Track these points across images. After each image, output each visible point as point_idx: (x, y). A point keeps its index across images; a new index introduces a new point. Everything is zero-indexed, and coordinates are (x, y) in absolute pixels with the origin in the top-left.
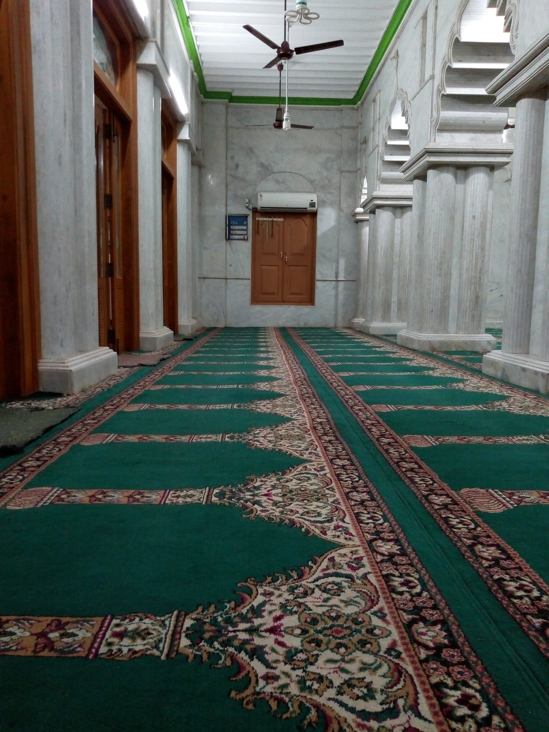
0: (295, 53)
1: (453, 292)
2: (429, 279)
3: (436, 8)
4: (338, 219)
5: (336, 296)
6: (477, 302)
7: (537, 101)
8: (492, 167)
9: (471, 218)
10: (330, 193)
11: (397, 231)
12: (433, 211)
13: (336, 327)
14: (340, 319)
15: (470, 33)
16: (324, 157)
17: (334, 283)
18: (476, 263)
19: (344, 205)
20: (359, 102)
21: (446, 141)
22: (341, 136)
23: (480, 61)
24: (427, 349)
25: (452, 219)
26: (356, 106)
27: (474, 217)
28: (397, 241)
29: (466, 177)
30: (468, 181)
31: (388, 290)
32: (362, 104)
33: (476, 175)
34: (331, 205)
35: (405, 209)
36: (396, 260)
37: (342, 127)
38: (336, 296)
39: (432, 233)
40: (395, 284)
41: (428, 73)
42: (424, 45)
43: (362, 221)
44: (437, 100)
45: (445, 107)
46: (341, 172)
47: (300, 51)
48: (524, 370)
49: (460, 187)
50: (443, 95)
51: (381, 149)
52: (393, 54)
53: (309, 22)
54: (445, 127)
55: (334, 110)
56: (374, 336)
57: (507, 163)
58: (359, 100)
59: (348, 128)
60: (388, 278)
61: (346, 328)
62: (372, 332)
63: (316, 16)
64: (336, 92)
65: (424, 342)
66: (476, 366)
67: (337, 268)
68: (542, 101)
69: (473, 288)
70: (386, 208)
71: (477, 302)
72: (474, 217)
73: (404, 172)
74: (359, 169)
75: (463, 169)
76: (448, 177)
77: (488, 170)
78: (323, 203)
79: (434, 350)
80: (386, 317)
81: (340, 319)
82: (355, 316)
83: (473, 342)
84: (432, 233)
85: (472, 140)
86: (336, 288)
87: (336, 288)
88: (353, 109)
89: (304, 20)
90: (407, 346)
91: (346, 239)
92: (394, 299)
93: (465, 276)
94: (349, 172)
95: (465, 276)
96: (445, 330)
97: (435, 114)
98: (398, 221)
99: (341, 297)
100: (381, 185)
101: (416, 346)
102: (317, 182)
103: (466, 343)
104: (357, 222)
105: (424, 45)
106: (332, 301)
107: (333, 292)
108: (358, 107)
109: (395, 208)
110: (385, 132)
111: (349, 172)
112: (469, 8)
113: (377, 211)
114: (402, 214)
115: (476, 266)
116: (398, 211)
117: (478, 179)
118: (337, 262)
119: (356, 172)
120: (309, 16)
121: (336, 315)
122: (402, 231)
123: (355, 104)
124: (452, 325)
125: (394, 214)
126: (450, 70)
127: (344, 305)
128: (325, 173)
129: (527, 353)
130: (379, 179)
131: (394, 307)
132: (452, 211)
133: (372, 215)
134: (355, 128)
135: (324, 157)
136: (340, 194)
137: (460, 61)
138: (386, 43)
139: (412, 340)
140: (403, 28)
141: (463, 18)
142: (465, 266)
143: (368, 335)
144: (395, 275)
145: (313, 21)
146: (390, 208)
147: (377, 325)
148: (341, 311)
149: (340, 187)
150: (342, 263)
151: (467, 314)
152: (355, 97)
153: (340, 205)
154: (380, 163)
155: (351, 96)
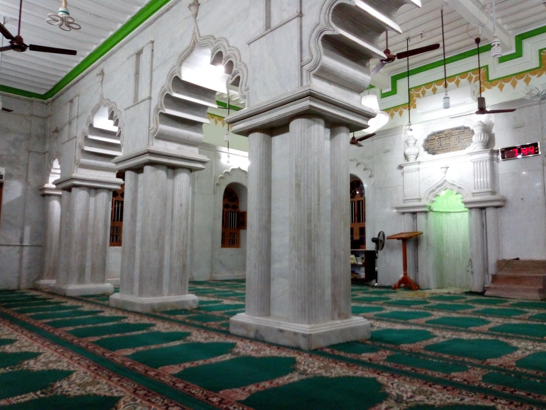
0: (28, 48)
1: (166, 262)
2: (149, 252)
3: (153, 51)
4: (25, 192)
5: (21, 259)
6: (184, 269)
7: (267, 136)
8: (191, 170)
9: (179, 205)
10: (18, 169)
11: (92, 207)
12: (151, 198)
13: (19, 289)
14: (24, 281)
15: (188, 75)
16: (12, 137)
17: (18, 248)
18: (183, 239)
19: (31, 180)
20: (50, 99)
21: (160, 146)
22: (31, 122)
23: (190, 96)
24: (149, 310)
25: (165, 205)
26: (46, 101)
27: (181, 205)
28: (91, 215)
29: (174, 175)
30: (176, 178)
31: (83, 256)
32: (53, 101)
33: (180, 175)
34: (19, 178)
35: (99, 190)
36: (90, 230)
37: (32, 115)
38: (21, 259)
39: (151, 215)
40: (89, 251)
41: (143, 94)
42: (137, 73)
43: (49, 195)
44: (155, 117)
45: (162, 122)
46: (29, 152)
47: (33, 48)
48: (281, 331)
49: (170, 181)
50: (161, 114)
51: (80, 140)
52: (97, 71)
53: (69, 29)
54: (162, 137)
55: (25, 100)
56: (71, 298)
57: (203, 169)
58: (50, 97)
59: (37, 117)
60: (84, 247)
61: (31, 289)
62: (68, 294)
63: (78, 27)
64: (31, 86)
65: (147, 305)
66: (106, 303)
67: (22, 234)
68: (269, 137)
69: (181, 259)
70: (83, 188)
71: (184, 269)
72: (181, 205)
73: (116, 163)
74: (47, 152)
75: (173, 169)
76: (162, 173)
77: (189, 171)
78: (10, 176)
79: (154, 311)
80: (81, 280)
81: (24, 281)
82: (40, 277)
83: (183, 302)
84: (151, 215)
85: (179, 148)
86: (21, 252)
87: (21, 252)
88: (43, 103)
89: (64, 27)
90: (125, 308)
91: (32, 210)
92: (88, 264)
93: (175, 250)
94: (37, 153)
95: (175, 250)
96: (161, 294)
97: (152, 125)
98: (92, 200)
99: (25, 261)
100: (79, 169)
101: (138, 309)
102: (4, 157)
103: (178, 303)
104: (44, 195)
105: (137, 73)
106: (16, 264)
107: (17, 256)
108: (49, 103)
109: (90, 188)
110: (87, 128)
111: (37, 153)
112: (188, 59)
113: (74, 189)
114: (96, 194)
115: (183, 242)
116: (93, 191)
117: (183, 178)
118: (23, 229)
119: (44, 153)
120: (71, 25)
121: (19, 277)
122: (96, 207)
123: (46, 99)
124: (166, 290)
125: (89, 192)
126: (168, 96)
127: (29, 268)
128: (13, 151)
129: (268, 315)
130: (77, 164)
131: (88, 270)
132: (166, 199)
133: (66, 193)
134: (45, 118)
135: (12, 137)
136: (27, 170)
137: (177, 92)
138: (90, 62)
139: (133, 304)
140: (110, 55)
141: (183, 64)
142: (175, 242)
143: (65, 296)
144: (89, 243)
145: (72, 29)
146: (86, 188)
147: (74, 287)
148: (25, 273)
149: (28, 164)
150: (28, 230)
151: (178, 279)
152: (46, 94)
153: (27, 180)
154: (78, 151)
155: (43, 93)
